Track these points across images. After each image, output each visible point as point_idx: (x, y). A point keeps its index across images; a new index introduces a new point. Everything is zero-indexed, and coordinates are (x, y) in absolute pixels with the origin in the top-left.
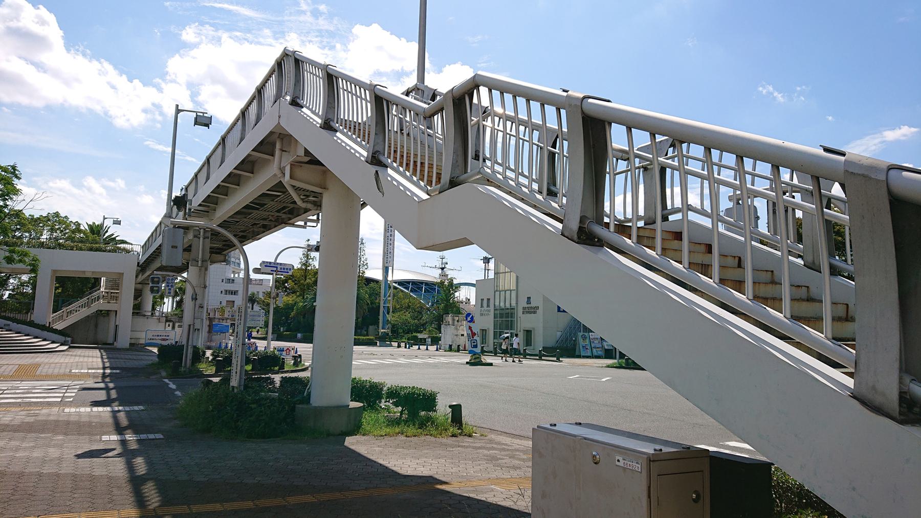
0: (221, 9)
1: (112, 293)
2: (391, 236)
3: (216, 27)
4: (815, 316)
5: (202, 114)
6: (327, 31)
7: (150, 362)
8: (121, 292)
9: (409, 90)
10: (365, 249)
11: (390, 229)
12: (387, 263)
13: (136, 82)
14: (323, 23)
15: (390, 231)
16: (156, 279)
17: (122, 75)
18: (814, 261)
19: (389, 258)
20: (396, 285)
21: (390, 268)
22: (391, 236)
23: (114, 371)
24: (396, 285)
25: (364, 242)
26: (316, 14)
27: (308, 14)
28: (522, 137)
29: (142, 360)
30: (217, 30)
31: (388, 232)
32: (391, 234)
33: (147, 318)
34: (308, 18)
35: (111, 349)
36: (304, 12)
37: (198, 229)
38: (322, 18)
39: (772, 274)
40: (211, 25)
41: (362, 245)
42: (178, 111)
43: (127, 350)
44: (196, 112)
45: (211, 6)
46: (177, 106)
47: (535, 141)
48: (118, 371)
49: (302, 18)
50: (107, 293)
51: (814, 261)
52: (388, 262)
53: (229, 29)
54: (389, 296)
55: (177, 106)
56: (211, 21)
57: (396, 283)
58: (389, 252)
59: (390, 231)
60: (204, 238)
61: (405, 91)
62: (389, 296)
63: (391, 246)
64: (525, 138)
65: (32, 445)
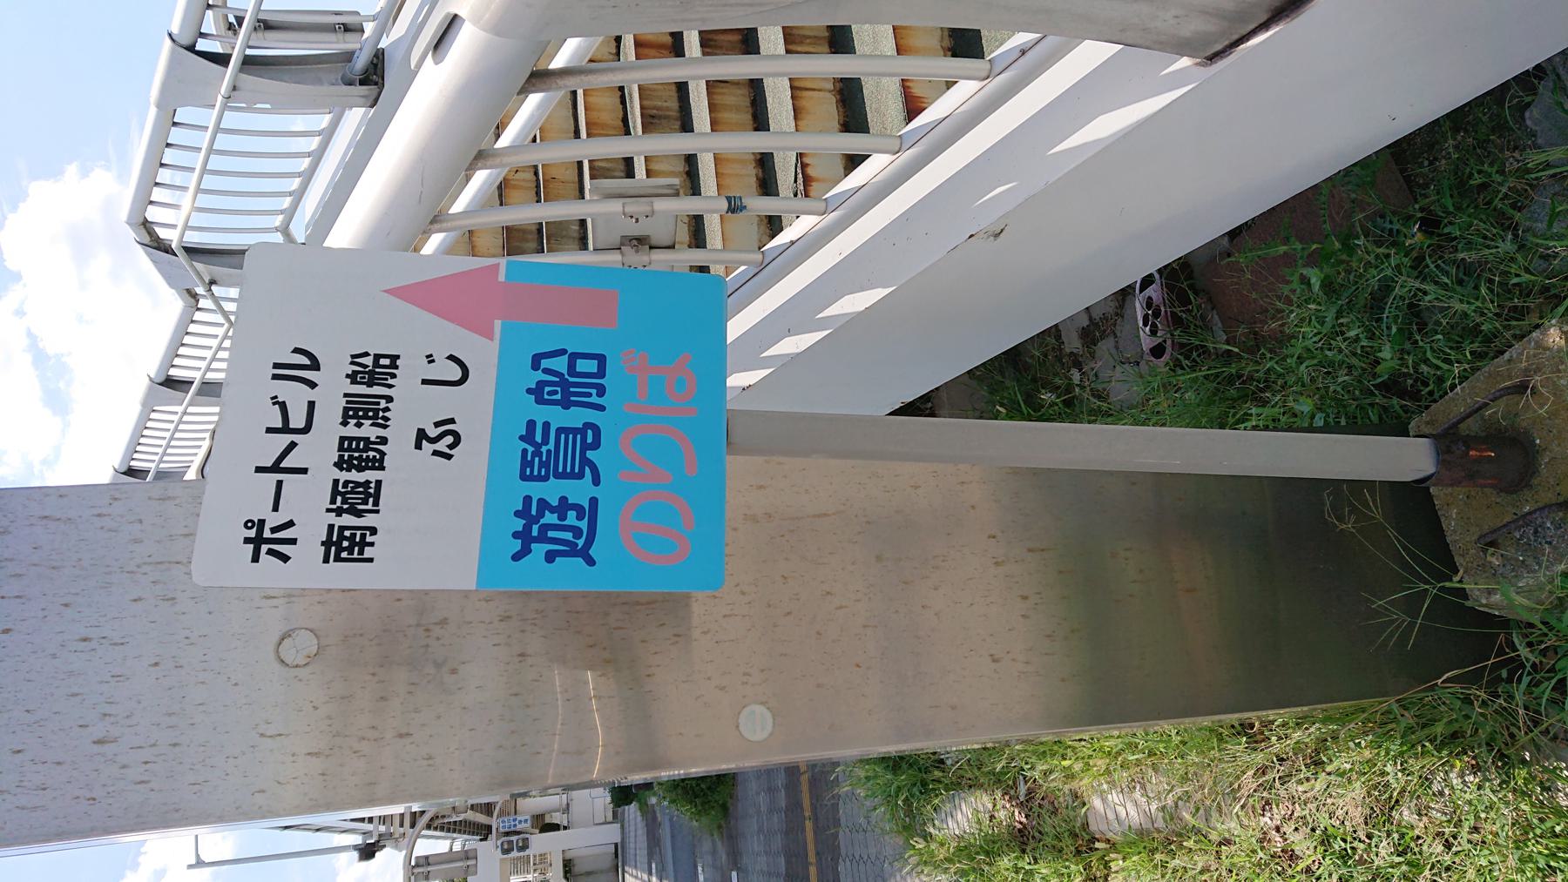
1: (534, 864)
7: (639, 813)
8: (589, 215)
9: (147, 240)
16: (506, 847)
18: (363, 96)
23: (654, 871)
28: (159, 456)
29: (636, 824)
33: (572, 800)
35: (623, 847)
37: (413, 878)
42: (200, 863)
43: (622, 827)
46: (190, 867)
47: (209, 117)
48: (654, 866)
50: (535, 870)
51: (363, 96)
55: (190, 867)
60: (429, 865)
61: (149, 255)
64: (205, 146)
65: (762, 809)
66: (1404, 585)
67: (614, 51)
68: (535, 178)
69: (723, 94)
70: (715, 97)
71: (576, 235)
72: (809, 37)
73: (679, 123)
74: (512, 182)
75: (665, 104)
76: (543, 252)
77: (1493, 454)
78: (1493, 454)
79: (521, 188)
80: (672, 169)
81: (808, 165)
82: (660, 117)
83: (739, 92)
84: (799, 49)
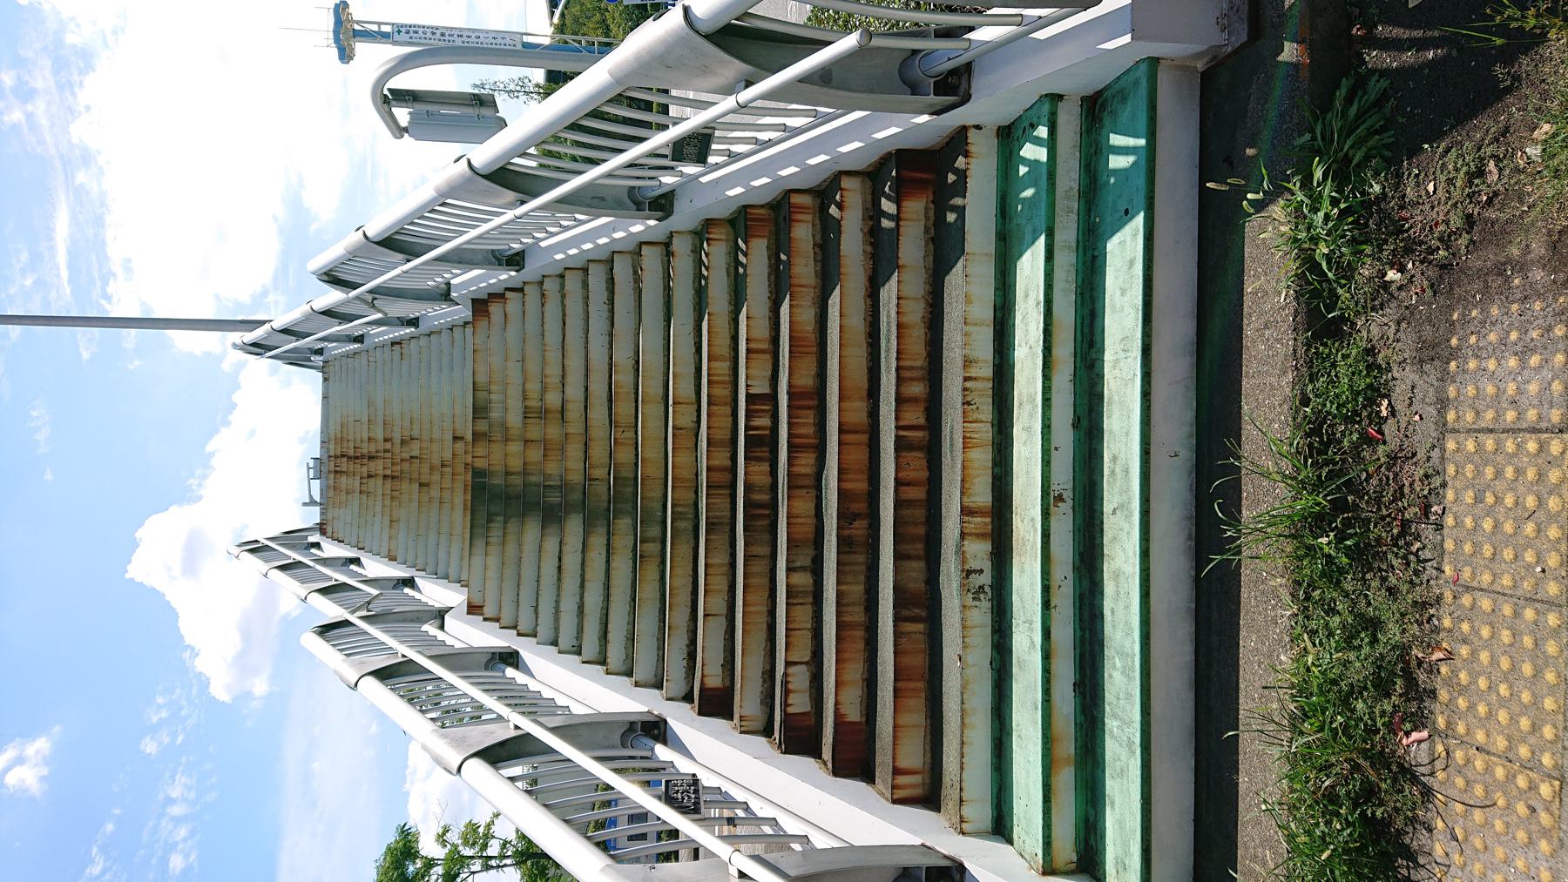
0: (70, 266)
2: (461, 36)
3: (108, 275)
4: (584, 339)
5: (311, 471)
6: (56, 72)
10: (492, 82)
11: (447, 38)
12: (514, 46)
13: (236, 398)
14: (42, 79)
15: (451, 38)
17: (229, 423)
19: (505, 41)
20: (558, 12)
21: (526, 39)
22: (461, 36)
24: (558, 12)
25: (478, 83)
26: (25, 94)
27: (29, 107)
30: (113, 274)
31: (454, 41)
32: (458, 36)
34: (39, 107)
36: (30, 116)
38: (30, 80)
39: (528, 283)
40: (105, 283)
41: (486, 86)
44: (309, 479)
45: (68, 283)
46: (305, 504)
49: (43, 121)
52: (513, 43)
53: (100, 244)
54: (580, 42)
55: (305, 504)
56: (98, 283)
57: (552, 13)
58: (493, 41)
59: (451, 38)
62: (580, 42)
63: (482, 35)
66: (850, 41)
67: (695, 419)
68: (635, 437)
69: (753, 565)
70: (749, 567)
71: (660, 519)
72: (801, 592)
73: (729, 527)
74: (619, 441)
75: (722, 514)
76: (652, 111)
77: (889, 183)
78: (889, 183)
79: (625, 444)
80: (721, 562)
81: (789, 682)
82: (718, 524)
83: (764, 562)
84: (795, 601)
